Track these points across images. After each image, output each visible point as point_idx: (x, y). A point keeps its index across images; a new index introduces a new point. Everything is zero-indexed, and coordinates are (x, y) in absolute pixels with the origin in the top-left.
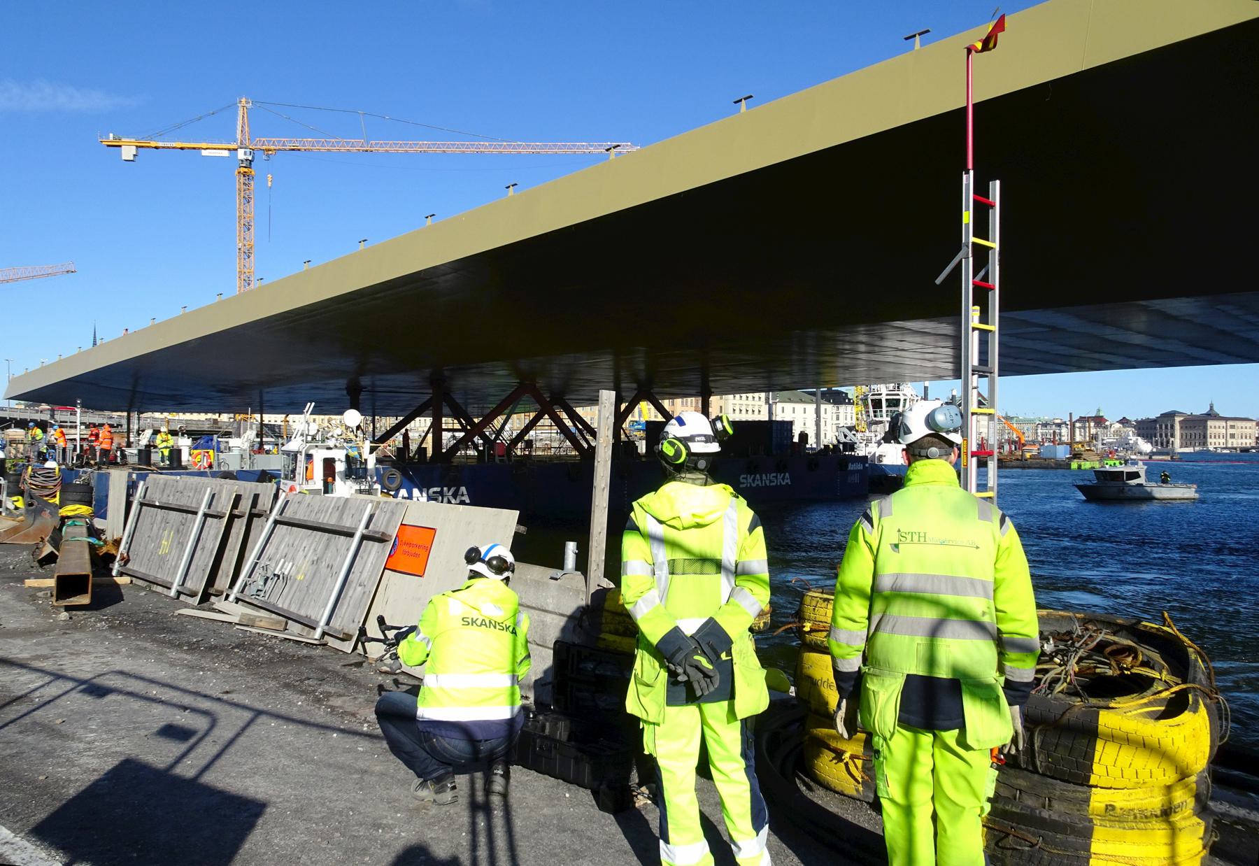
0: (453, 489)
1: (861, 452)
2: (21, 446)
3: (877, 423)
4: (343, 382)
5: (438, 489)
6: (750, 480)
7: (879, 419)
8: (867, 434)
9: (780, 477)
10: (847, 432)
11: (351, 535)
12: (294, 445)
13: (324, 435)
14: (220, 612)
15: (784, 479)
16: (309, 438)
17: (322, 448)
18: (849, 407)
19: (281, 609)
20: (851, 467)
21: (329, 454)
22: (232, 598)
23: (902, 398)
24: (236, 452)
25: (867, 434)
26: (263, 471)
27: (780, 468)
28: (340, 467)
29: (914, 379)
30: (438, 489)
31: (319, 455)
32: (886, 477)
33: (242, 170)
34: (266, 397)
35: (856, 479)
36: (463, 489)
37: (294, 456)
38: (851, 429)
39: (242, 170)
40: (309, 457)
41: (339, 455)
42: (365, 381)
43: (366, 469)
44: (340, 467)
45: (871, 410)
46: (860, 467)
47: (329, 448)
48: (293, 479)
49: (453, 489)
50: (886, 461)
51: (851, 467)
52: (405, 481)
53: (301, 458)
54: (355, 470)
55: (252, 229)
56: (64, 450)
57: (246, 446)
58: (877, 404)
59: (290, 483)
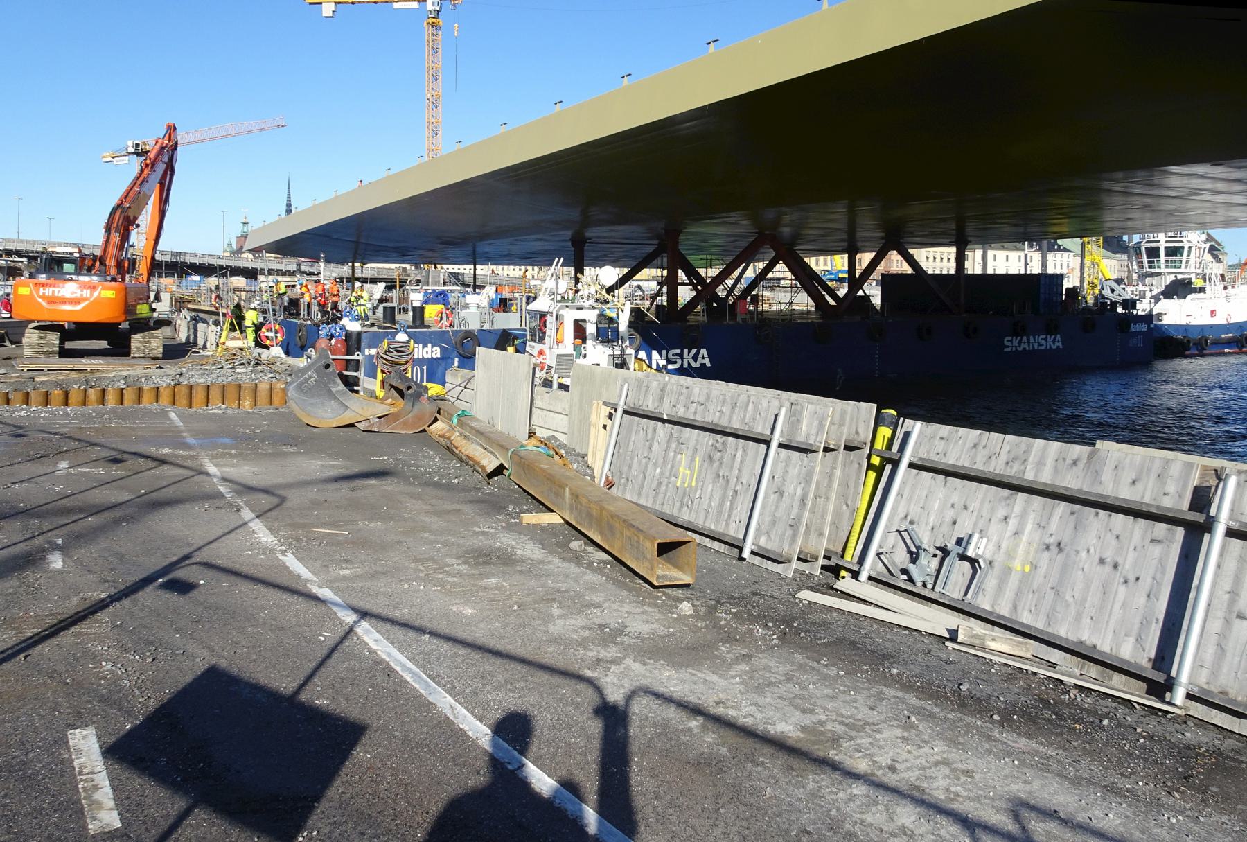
0: (694, 351)
1: (1142, 308)
2: (243, 294)
3: (1152, 275)
4: (568, 234)
5: (678, 351)
6: (1015, 343)
7: (1157, 270)
8: (1141, 288)
9: (1050, 339)
10: (1114, 285)
11: (911, 466)
12: (540, 305)
13: (575, 296)
14: (860, 600)
15: (1055, 343)
16: (559, 298)
17: (572, 308)
18: (1059, 254)
19: (1001, 617)
20: (1134, 328)
21: (580, 315)
22: (863, 576)
23: (1186, 246)
24: (473, 309)
25: (1141, 288)
26: (504, 331)
27: (1051, 330)
28: (591, 329)
29: (1202, 226)
30: (678, 351)
31: (570, 316)
32: (1170, 339)
33: (431, 21)
34: (479, 250)
35: (1138, 342)
36: (703, 352)
37: (543, 316)
38: (1119, 281)
39: (431, 21)
40: (559, 317)
41: (590, 316)
42: (591, 233)
43: (616, 331)
44: (591, 329)
45: (1145, 260)
46: (1144, 328)
47: (580, 308)
48: (542, 340)
49: (694, 351)
50: (1166, 320)
51: (1134, 328)
52: (644, 345)
53: (551, 320)
54: (607, 334)
55: (440, 79)
56: (309, 305)
57: (485, 303)
58: (1153, 253)
59: (538, 346)
